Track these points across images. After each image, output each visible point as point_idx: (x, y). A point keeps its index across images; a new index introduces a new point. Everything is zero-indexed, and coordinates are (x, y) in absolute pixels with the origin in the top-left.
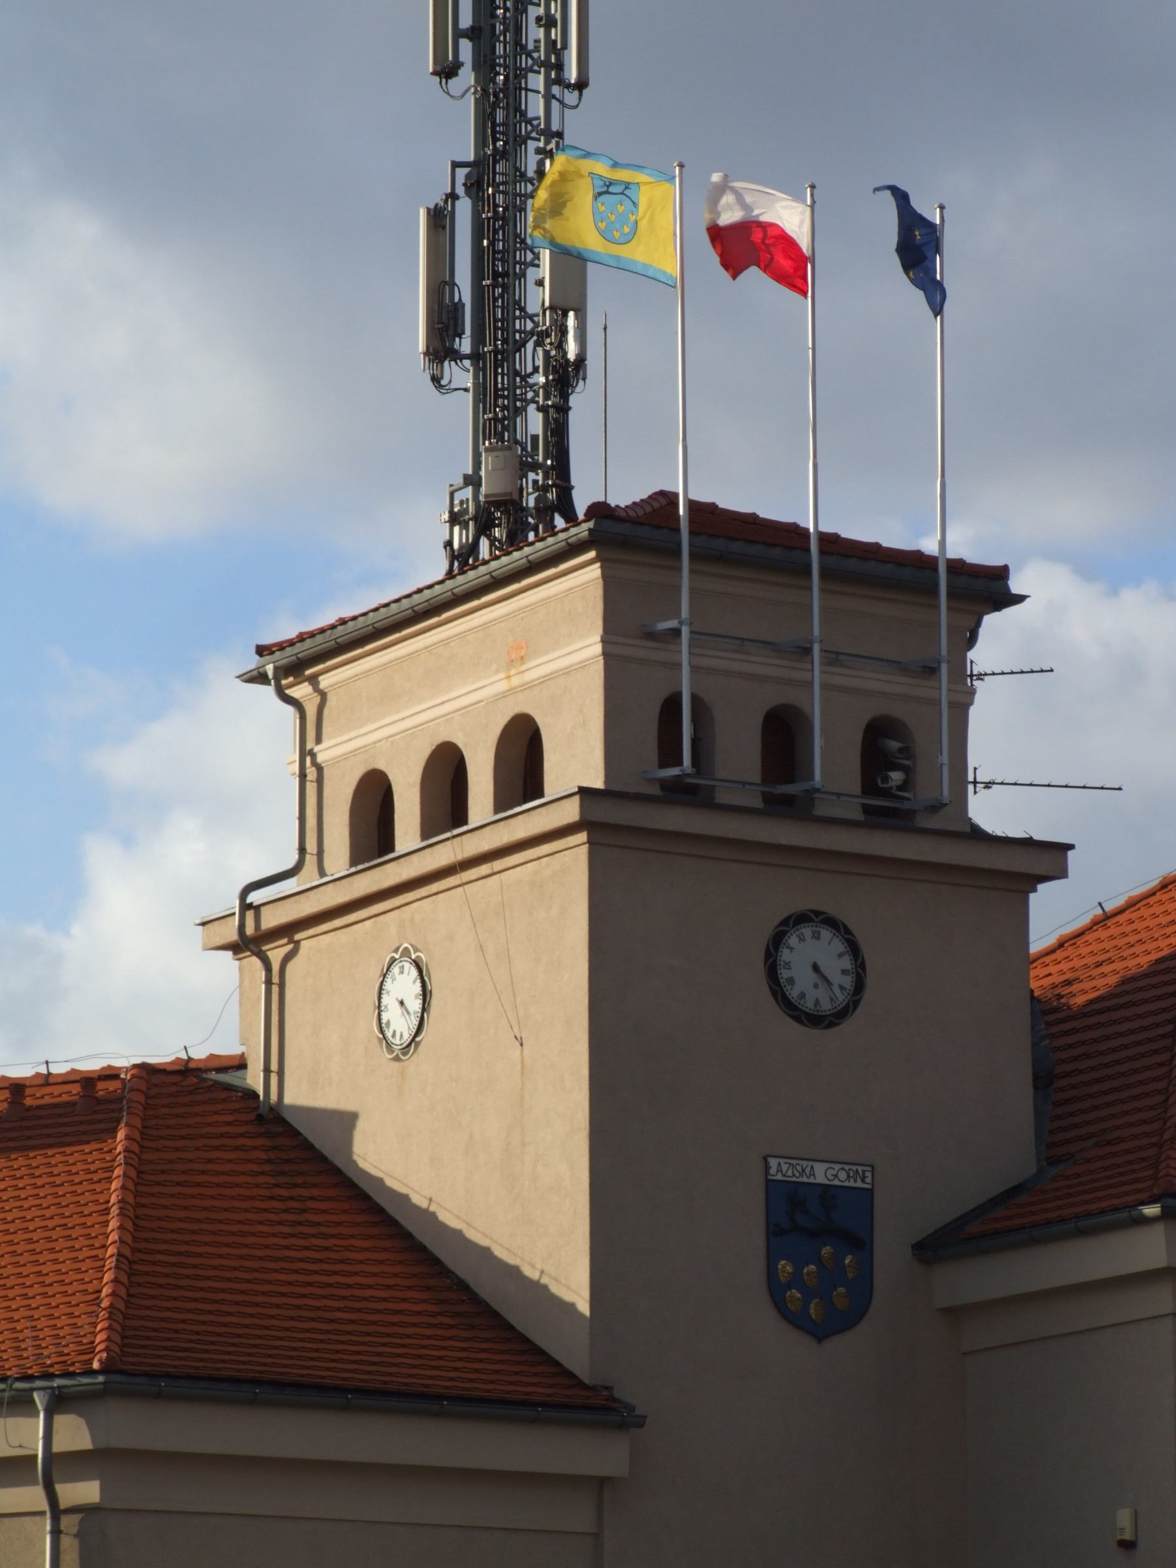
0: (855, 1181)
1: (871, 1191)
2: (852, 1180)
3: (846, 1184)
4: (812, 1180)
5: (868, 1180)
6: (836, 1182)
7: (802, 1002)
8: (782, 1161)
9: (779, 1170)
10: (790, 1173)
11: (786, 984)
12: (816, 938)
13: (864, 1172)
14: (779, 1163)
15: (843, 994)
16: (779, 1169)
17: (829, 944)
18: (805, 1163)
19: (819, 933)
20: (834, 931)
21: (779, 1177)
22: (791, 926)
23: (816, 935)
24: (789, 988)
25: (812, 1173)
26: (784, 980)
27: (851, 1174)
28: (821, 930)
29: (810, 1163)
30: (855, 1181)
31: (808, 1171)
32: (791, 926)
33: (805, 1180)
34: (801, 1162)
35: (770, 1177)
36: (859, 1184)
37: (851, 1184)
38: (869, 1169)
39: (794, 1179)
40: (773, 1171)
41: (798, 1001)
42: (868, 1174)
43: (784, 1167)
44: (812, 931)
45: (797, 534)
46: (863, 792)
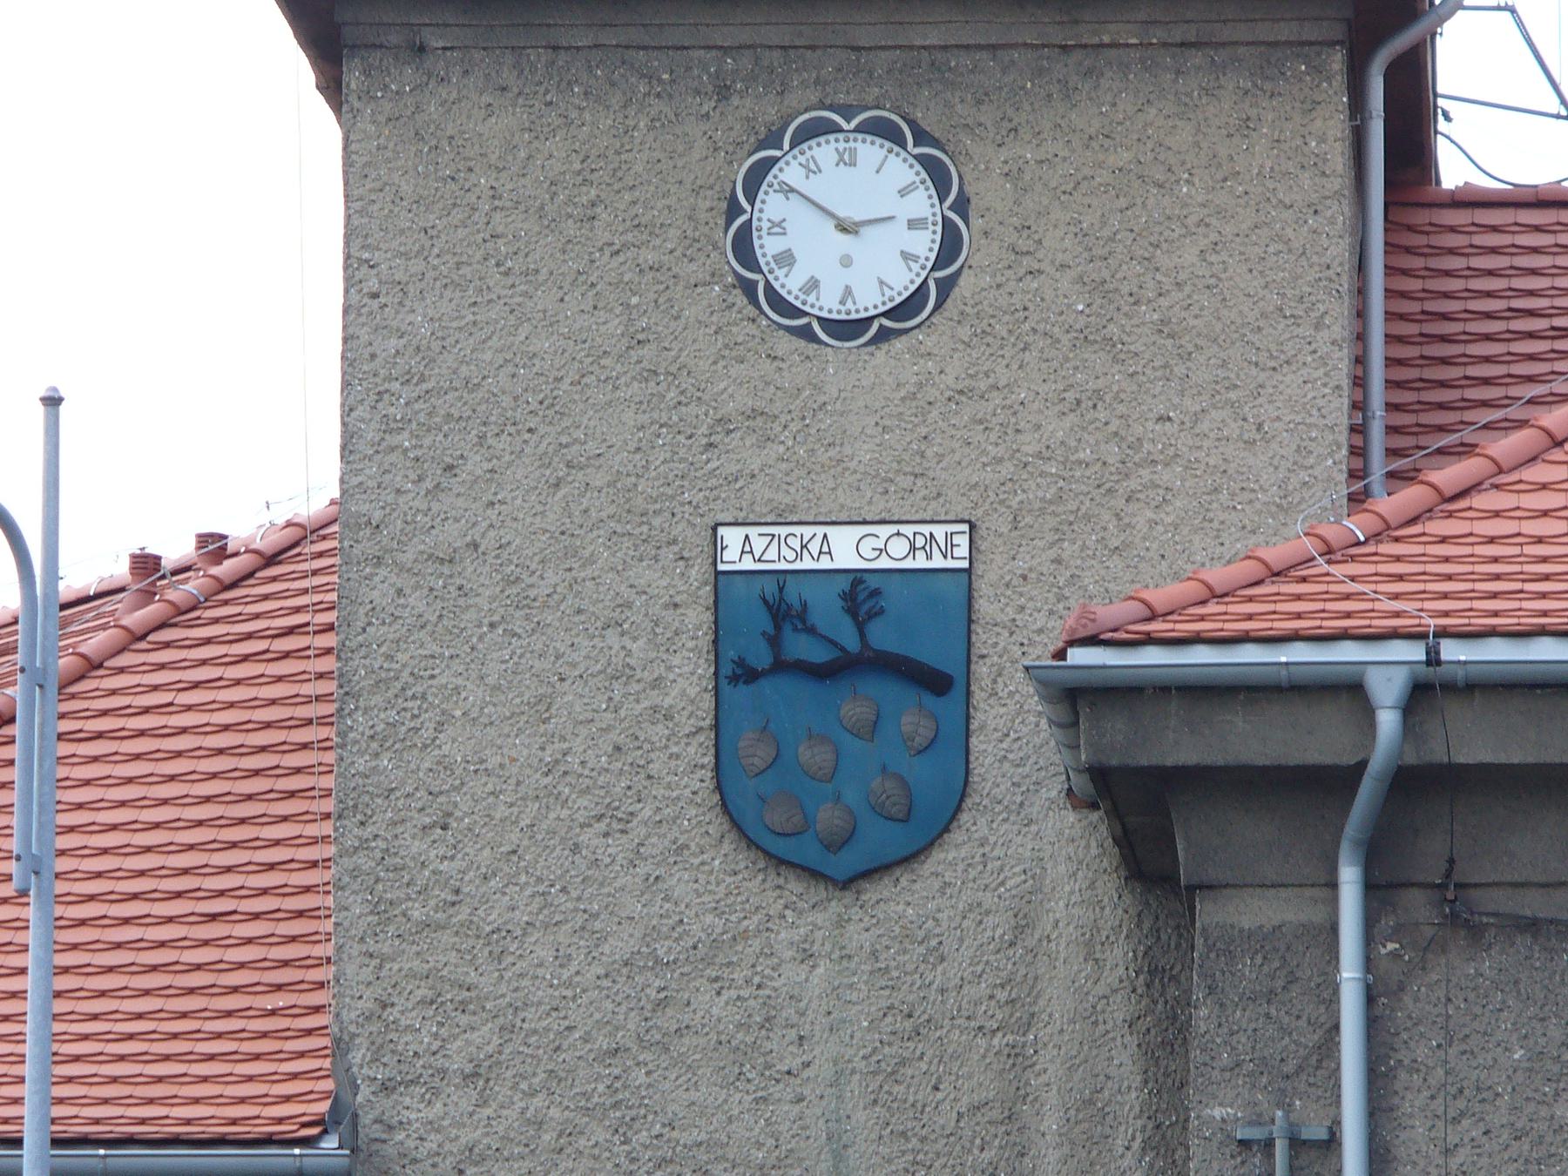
0: (929, 557)
1: (969, 571)
2: (920, 555)
3: (908, 564)
4: (825, 564)
5: (963, 550)
6: (884, 563)
7: (811, 299)
8: (753, 532)
9: (747, 547)
10: (772, 554)
11: (773, 265)
12: (845, 164)
13: (949, 537)
14: (747, 536)
15: (910, 270)
16: (747, 548)
17: (877, 172)
18: (807, 531)
19: (853, 152)
20: (888, 144)
21: (748, 564)
22: (786, 146)
23: (846, 157)
24: (780, 273)
25: (825, 549)
26: (769, 258)
27: (920, 542)
28: (859, 145)
29: (820, 530)
30: (929, 557)
31: (814, 547)
32: (786, 146)
33: (807, 564)
34: (797, 530)
35: (721, 567)
36: (938, 562)
37: (920, 562)
38: (965, 527)
39: (783, 566)
40: (732, 553)
41: (802, 297)
42: (963, 541)
43: (759, 545)
44: (837, 149)
45: (722, 47)
46: (1362, 675)
